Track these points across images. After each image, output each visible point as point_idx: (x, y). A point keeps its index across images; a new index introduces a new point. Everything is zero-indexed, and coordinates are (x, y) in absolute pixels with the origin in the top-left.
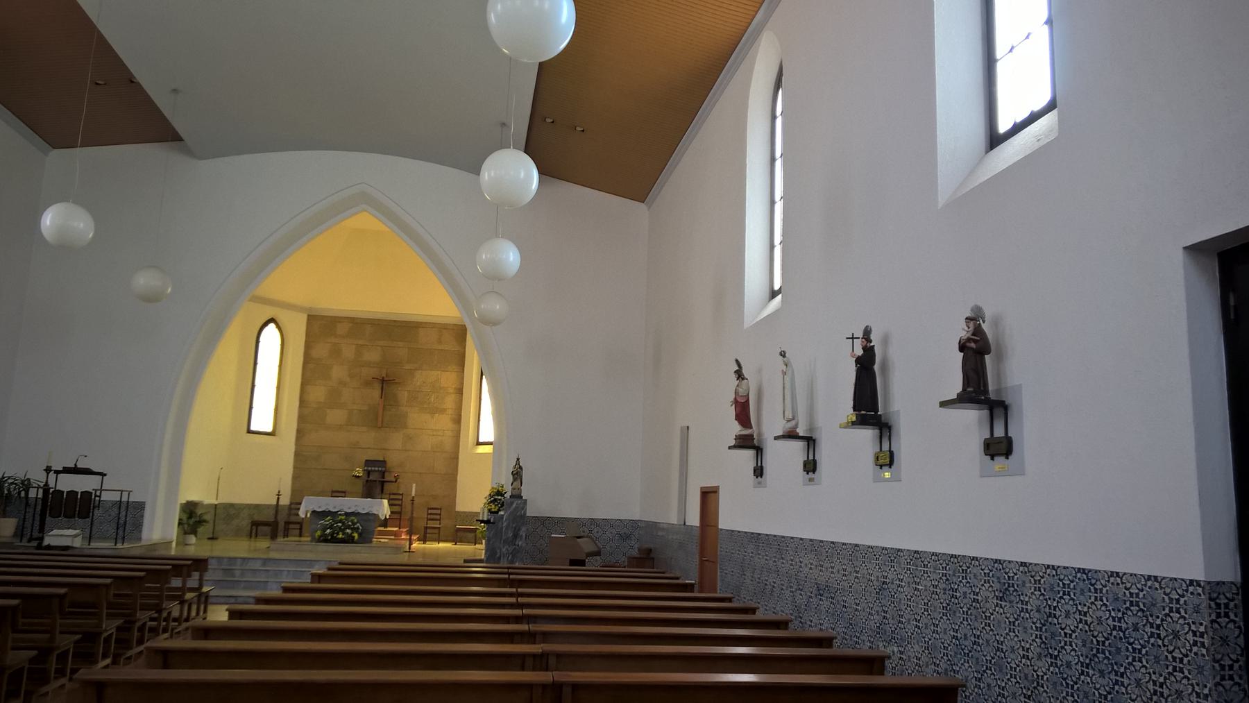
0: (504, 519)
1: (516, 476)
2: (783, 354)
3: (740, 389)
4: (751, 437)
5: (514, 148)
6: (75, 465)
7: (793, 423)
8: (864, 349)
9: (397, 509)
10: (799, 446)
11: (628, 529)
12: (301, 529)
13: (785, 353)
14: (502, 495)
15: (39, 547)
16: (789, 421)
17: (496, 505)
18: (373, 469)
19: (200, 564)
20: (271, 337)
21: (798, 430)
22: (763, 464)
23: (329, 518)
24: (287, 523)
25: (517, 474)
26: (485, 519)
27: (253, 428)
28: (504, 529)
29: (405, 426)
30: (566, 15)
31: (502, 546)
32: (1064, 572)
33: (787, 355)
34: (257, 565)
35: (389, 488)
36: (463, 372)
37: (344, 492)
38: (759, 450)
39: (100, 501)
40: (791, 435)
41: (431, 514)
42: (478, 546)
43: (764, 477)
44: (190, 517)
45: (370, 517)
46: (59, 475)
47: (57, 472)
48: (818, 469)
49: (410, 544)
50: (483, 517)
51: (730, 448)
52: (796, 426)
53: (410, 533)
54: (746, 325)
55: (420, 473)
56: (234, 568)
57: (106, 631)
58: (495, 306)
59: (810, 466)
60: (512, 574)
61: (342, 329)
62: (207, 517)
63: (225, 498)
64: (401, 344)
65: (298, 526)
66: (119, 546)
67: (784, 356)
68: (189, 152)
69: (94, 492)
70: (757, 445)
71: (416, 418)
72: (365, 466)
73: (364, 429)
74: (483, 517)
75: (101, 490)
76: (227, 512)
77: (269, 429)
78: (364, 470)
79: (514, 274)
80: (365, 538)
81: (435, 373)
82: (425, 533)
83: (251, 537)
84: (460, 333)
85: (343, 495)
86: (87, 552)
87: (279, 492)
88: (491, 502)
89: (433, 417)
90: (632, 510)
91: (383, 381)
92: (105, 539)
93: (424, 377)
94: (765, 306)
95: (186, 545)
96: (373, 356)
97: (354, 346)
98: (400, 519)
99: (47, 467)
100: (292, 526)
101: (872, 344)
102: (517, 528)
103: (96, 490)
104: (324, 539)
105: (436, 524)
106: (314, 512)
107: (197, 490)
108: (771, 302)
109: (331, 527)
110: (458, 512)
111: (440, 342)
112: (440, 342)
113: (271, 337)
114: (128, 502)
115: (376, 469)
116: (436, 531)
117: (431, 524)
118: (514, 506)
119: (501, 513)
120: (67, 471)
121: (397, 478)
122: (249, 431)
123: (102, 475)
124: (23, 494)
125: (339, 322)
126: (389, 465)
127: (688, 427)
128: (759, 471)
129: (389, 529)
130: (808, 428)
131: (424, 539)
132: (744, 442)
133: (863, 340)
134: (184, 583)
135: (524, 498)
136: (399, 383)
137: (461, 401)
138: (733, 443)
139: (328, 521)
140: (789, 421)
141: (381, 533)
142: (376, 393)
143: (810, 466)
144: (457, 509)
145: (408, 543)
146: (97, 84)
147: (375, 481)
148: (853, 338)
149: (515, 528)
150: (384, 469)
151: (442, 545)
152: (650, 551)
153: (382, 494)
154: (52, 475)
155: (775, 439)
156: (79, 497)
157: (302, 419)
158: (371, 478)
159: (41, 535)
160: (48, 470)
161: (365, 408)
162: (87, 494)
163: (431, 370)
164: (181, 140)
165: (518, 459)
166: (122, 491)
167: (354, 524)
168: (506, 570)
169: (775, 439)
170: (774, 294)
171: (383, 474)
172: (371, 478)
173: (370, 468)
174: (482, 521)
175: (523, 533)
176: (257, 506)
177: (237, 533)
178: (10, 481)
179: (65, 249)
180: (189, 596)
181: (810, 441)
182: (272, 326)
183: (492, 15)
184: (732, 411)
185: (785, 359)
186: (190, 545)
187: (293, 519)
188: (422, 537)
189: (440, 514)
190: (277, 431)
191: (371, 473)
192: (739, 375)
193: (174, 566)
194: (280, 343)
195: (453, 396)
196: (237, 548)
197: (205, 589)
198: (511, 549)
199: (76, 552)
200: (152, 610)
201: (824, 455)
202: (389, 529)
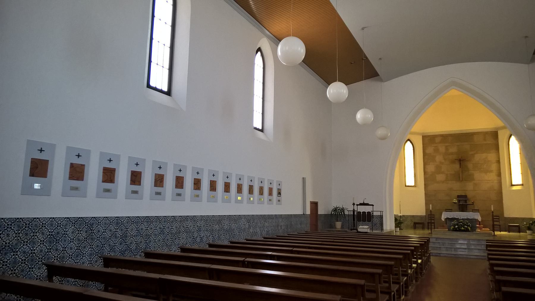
6: (364, 202)
18: (461, 199)
20: (408, 147)
23: (455, 221)
27: (407, 185)
32: (73, 219)
37: (452, 210)
46: (358, 206)
47: (357, 205)
61: (438, 140)
68: (381, 80)
71: (477, 175)
72: (458, 198)
75: (373, 211)
77: (413, 184)
78: (457, 200)
83: (414, 229)
85: (451, 211)
91: (460, 160)
92: (376, 229)
97: (444, 147)
103: (372, 211)
104: (455, 230)
109: (457, 225)
113: (408, 147)
115: (463, 199)
120: (361, 204)
122: (406, 186)
123: (373, 205)
142: (457, 166)
150: (466, 199)
151: (502, 233)
154: (355, 206)
156: (366, 214)
157: (425, 179)
160: (354, 204)
162: (369, 213)
166: (381, 211)
167: (467, 223)
171: (466, 201)
173: (460, 199)
176: (413, 216)
179: (365, 126)
186: (398, 232)
191: (460, 201)
194: (413, 149)
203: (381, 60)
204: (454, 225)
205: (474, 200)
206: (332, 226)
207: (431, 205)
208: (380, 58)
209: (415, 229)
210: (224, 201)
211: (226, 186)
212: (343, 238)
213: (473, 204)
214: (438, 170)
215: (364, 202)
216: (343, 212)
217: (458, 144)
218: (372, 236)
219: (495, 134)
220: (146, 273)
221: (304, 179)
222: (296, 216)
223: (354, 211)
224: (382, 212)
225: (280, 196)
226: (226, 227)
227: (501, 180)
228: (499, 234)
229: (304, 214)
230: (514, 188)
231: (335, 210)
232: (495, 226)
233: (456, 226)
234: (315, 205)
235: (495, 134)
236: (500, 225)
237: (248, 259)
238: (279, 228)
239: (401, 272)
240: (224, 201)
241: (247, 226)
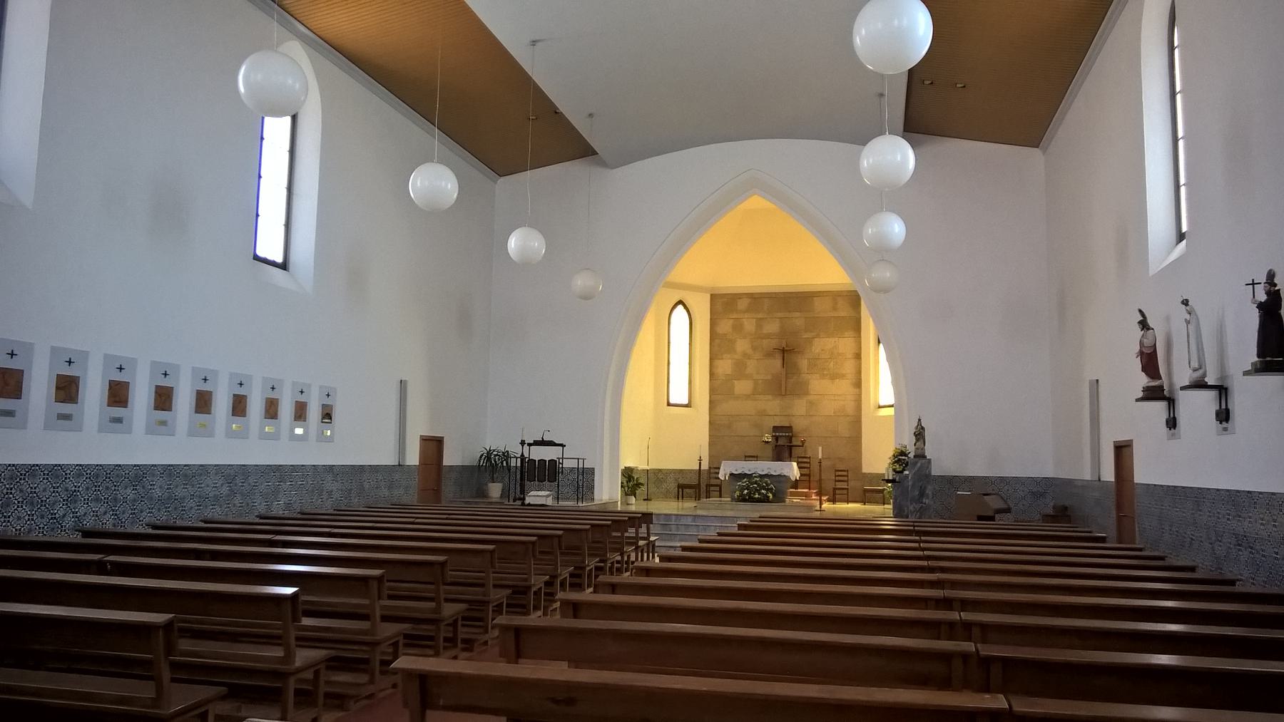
0: (910, 478)
2: (1186, 303)
3: (1145, 340)
5: (889, 134)
6: (542, 438)
7: (1201, 372)
8: (1268, 293)
9: (806, 471)
10: (1210, 395)
11: (1042, 487)
12: (720, 491)
13: (1187, 300)
14: (906, 455)
15: (523, 504)
16: (1195, 370)
17: (900, 465)
19: (647, 518)
21: (1206, 380)
22: (1230, 407)
24: (708, 486)
25: (920, 435)
26: (891, 478)
28: (910, 487)
29: (807, 393)
30: (921, 28)
31: (909, 504)
34: (689, 521)
35: (796, 451)
36: (860, 337)
37: (757, 457)
38: (1171, 402)
39: (562, 467)
40: (1199, 385)
41: (838, 476)
42: (886, 506)
43: (1230, 422)
44: (629, 481)
45: (782, 478)
46: (531, 447)
47: (530, 445)
48: (1177, 425)
49: (821, 504)
51: (1137, 400)
52: (1204, 375)
53: (820, 494)
54: (1151, 273)
56: (670, 523)
57: (588, 566)
58: (885, 274)
59: (1224, 416)
60: (917, 526)
61: (743, 304)
62: (641, 481)
63: (654, 465)
64: (798, 314)
65: (718, 489)
66: (580, 504)
68: (604, 164)
70: (1168, 396)
71: (817, 385)
73: (770, 397)
75: (563, 458)
76: (657, 476)
79: (902, 242)
80: (779, 498)
82: (834, 494)
84: (854, 299)
85: (755, 459)
86: (557, 508)
88: (896, 462)
90: (1048, 470)
91: (783, 351)
92: (567, 499)
93: (822, 345)
94: (1169, 253)
95: (628, 504)
96: (772, 327)
98: (809, 481)
99: (522, 441)
100: (712, 488)
101: (1277, 288)
102: (923, 488)
103: (559, 459)
104: (742, 499)
105: (843, 485)
106: (732, 474)
107: (632, 458)
108: (1178, 246)
110: (865, 473)
111: (835, 309)
112: (835, 309)
114: (583, 468)
115: (784, 434)
116: (845, 492)
117: (839, 485)
118: (919, 465)
119: (906, 472)
120: (537, 443)
121: (803, 442)
122: (669, 404)
124: (505, 464)
125: (740, 298)
126: (795, 429)
127: (1097, 380)
128: (1171, 423)
129: (799, 490)
130: (1219, 376)
131: (833, 501)
132: (1152, 394)
133: (1266, 285)
134: (637, 533)
135: (928, 458)
137: (860, 365)
138: (1141, 395)
139: (744, 482)
140: (1195, 370)
141: (793, 494)
142: (778, 362)
143: (1224, 416)
144: (864, 471)
145: (818, 503)
147: (784, 446)
148: (1253, 284)
150: (791, 434)
151: (851, 505)
152: (1065, 508)
153: (790, 458)
155: (1244, 375)
157: (713, 391)
158: (780, 443)
159: (522, 496)
160: (523, 443)
161: (769, 377)
163: (829, 337)
164: (594, 153)
165: (920, 420)
166: (578, 459)
167: (767, 485)
168: (912, 524)
169: (1244, 375)
170: (1181, 237)
171: (790, 438)
172: (780, 443)
173: (777, 434)
174: (888, 481)
175: (929, 491)
177: (666, 496)
178: (495, 453)
180: (641, 543)
181: (1222, 391)
182: (680, 307)
183: (858, 38)
184: (1137, 364)
185: (1188, 308)
186: (631, 504)
187: (714, 482)
188: (831, 498)
189: (847, 476)
190: (692, 403)
191: (779, 439)
192: (1144, 324)
193: (630, 518)
195: (853, 361)
196: (660, 507)
197: (652, 538)
198: (918, 506)
200: (618, 552)
201: (1238, 404)
202: (799, 490)
203: (592, 117)
204: (742, 489)
205: (806, 437)
206: (482, 493)
207: (820, 448)
209: (680, 498)
210: (230, 434)
211: (160, 395)
214: (740, 370)
215: (542, 438)
216: (505, 462)
217: (780, 315)
218: (600, 514)
220: (564, 665)
221: (403, 384)
222: (375, 469)
224: (583, 459)
225: (331, 423)
226: (157, 492)
227: (860, 395)
228: (846, 508)
229: (399, 465)
232: (837, 492)
234: (433, 446)
236: (847, 489)
237: (112, 558)
238: (325, 496)
239: (491, 581)
240: (230, 434)
241: (225, 490)
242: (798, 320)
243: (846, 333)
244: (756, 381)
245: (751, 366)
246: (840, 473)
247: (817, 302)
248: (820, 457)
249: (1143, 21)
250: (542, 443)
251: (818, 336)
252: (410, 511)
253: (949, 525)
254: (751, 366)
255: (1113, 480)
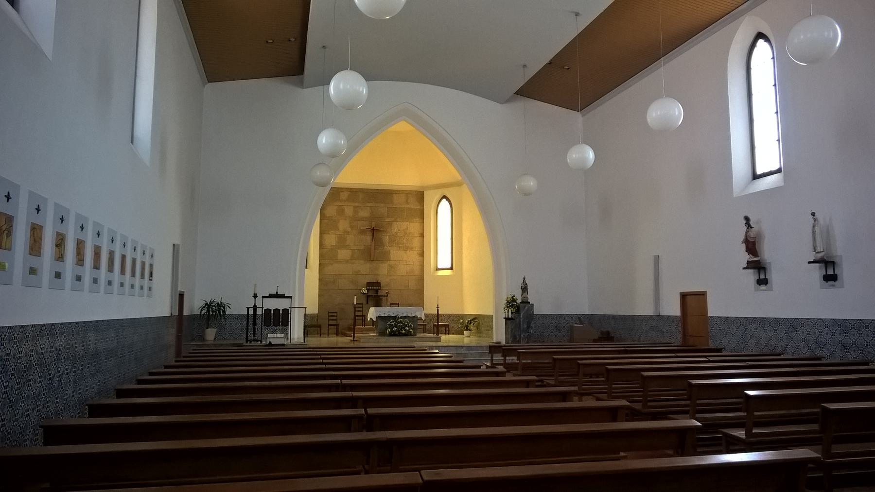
1: (524, 289)
2: (813, 214)
4: (758, 262)
13: (814, 213)
25: (525, 289)
33: (816, 215)
47: (263, 297)
50: (508, 316)
55: (400, 290)
61: (344, 196)
64: (382, 205)
67: (814, 216)
69: (290, 309)
71: (395, 254)
73: (362, 262)
74: (508, 316)
81: (406, 224)
87: (438, 305)
89: (405, 253)
93: (399, 227)
96: (364, 213)
99: (254, 294)
111: (407, 203)
112: (407, 203)
120: (271, 296)
122: (451, 268)
123: (291, 297)
136: (383, 231)
142: (369, 238)
146: (267, 42)
149: (528, 322)
157: (321, 256)
160: (255, 296)
161: (362, 248)
165: (524, 279)
171: (377, 291)
175: (532, 325)
195: (418, 238)
199: (285, 347)
208: (325, 45)
212: (328, 366)
213: (387, 296)
214: (342, 243)
215: (277, 292)
217: (369, 205)
219: (420, 196)
223: (255, 308)
224: (329, 313)
230: (440, 273)
231: (208, 306)
233: (395, 329)
235: (420, 196)
242: (383, 209)
243: (414, 220)
244: (353, 250)
245: (350, 240)
246: (332, 314)
247: (395, 197)
248: (355, 303)
249: (730, 53)
250: (277, 296)
251: (395, 221)
252: (279, 357)
253: (246, 350)
254: (350, 240)
255: (680, 315)
